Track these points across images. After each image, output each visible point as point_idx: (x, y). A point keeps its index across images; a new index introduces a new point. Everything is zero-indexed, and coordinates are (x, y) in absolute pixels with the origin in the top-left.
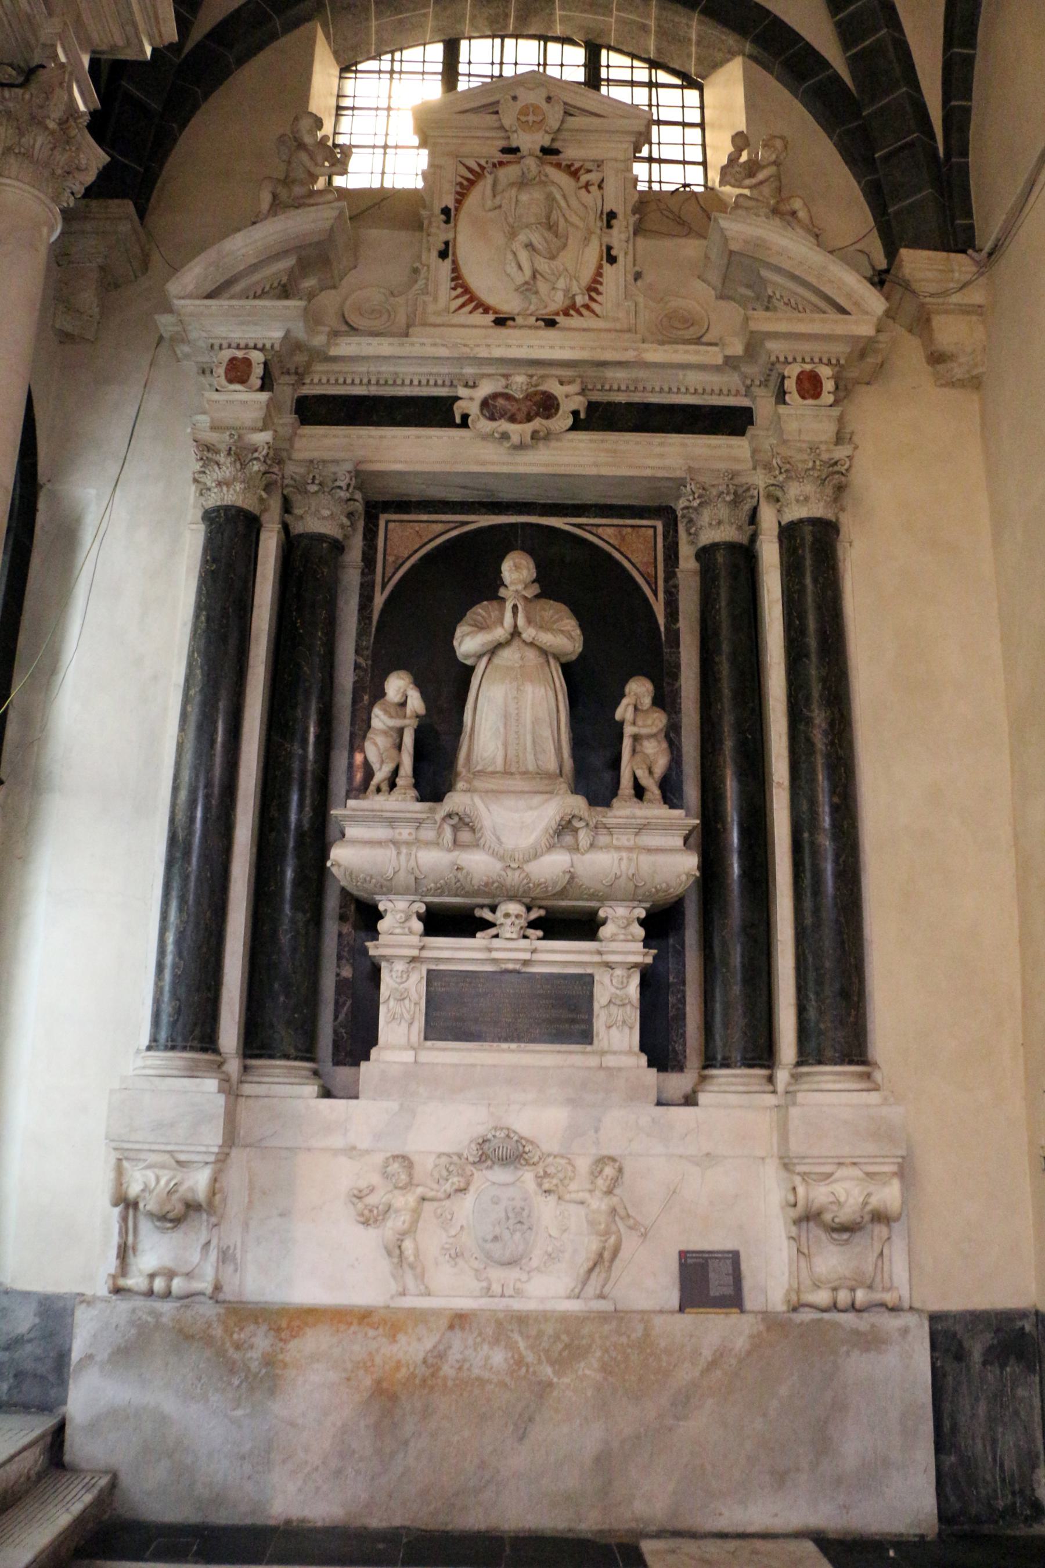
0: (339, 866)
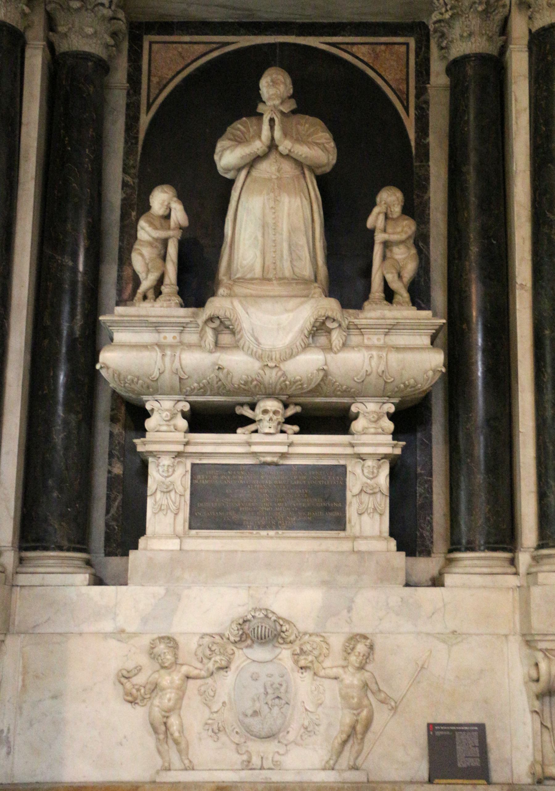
0: (108, 368)
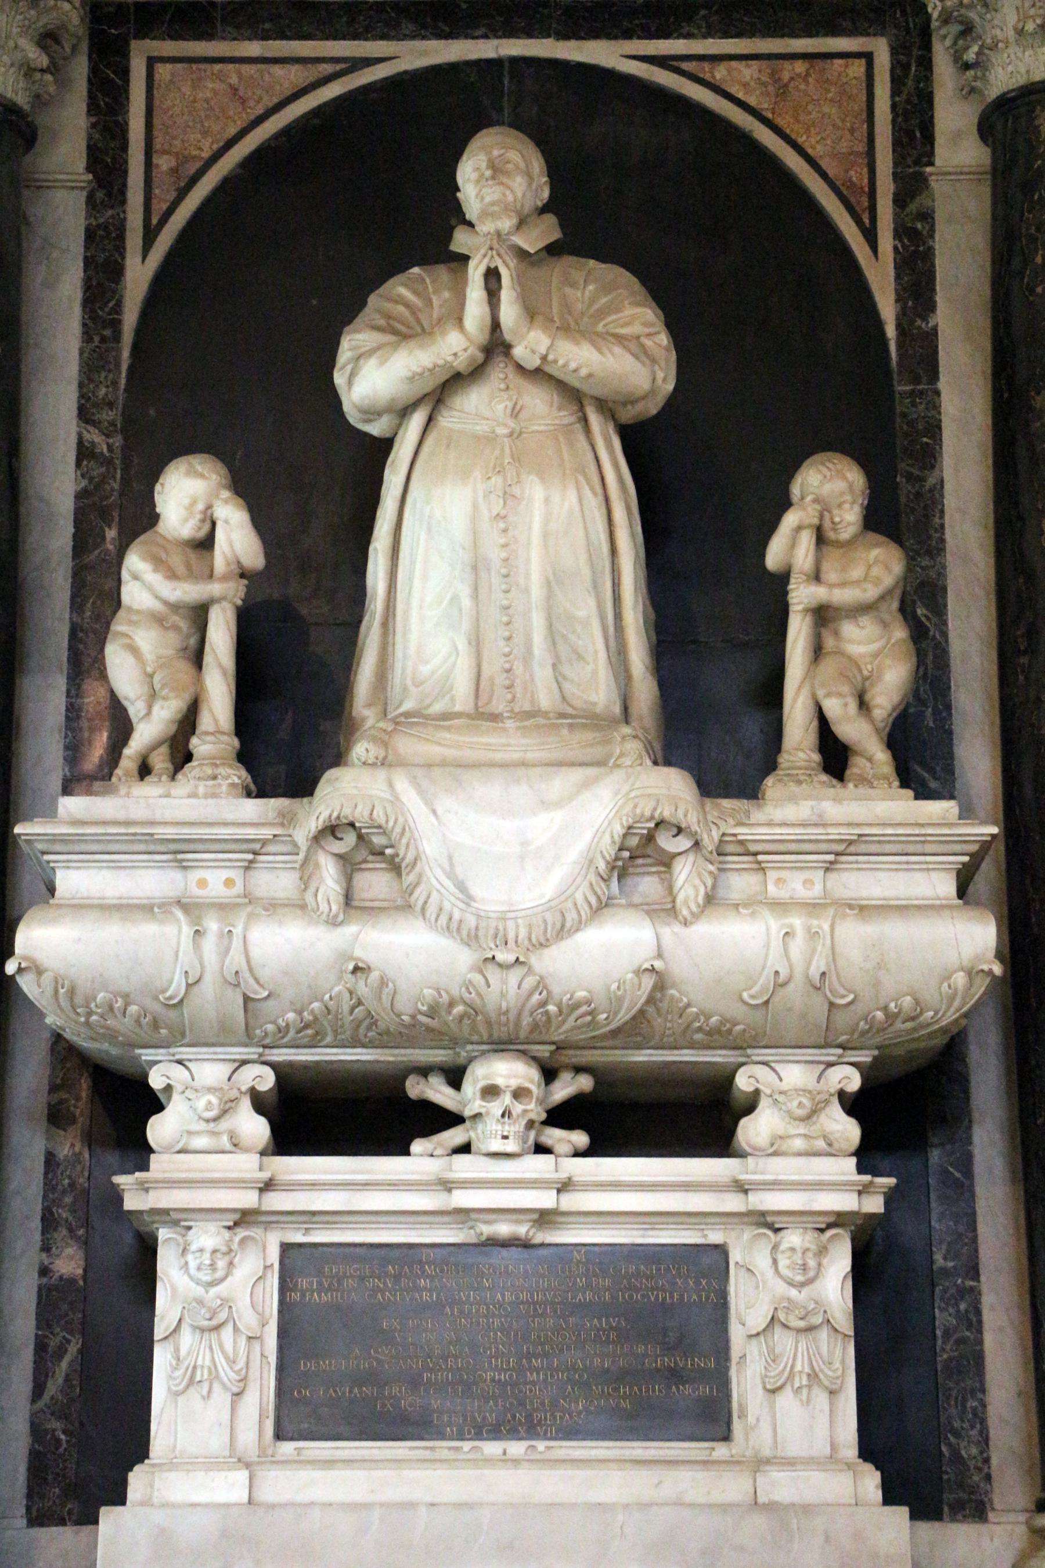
0: (39, 971)
